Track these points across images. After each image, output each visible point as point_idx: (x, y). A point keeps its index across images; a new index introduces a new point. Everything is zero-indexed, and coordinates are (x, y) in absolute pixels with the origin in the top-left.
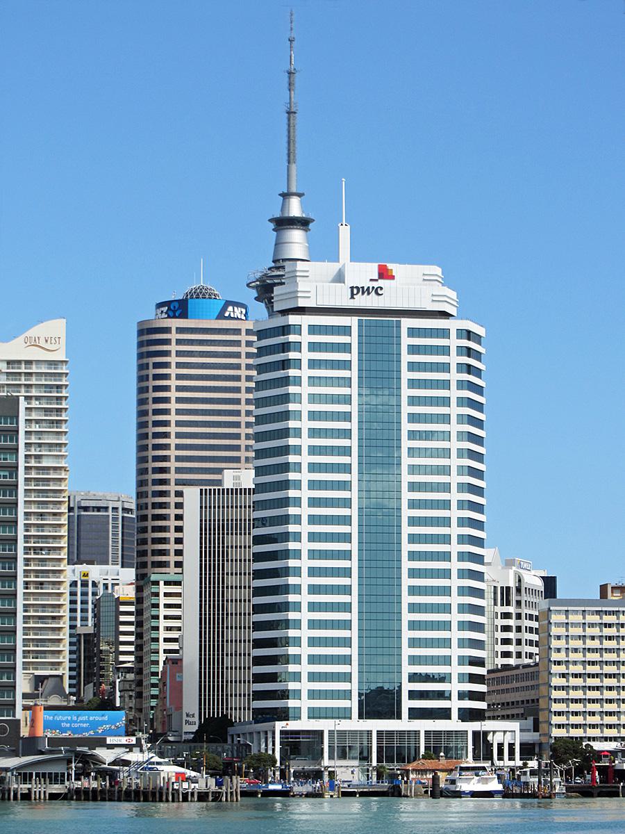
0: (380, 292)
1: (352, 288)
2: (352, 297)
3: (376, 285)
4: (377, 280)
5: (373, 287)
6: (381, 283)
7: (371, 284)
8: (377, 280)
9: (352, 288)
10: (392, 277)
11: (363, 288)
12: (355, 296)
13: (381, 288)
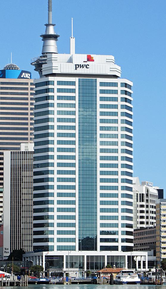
0: (88, 67)
1: (76, 65)
2: (76, 69)
3: (86, 64)
4: (86, 62)
5: (85, 65)
6: (88, 63)
7: (84, 63)
8: (86, 62)
9: (76, 65)
10: (93, 61)
11: (80, 65)
12: (77, 69)
13: (88, 65)
